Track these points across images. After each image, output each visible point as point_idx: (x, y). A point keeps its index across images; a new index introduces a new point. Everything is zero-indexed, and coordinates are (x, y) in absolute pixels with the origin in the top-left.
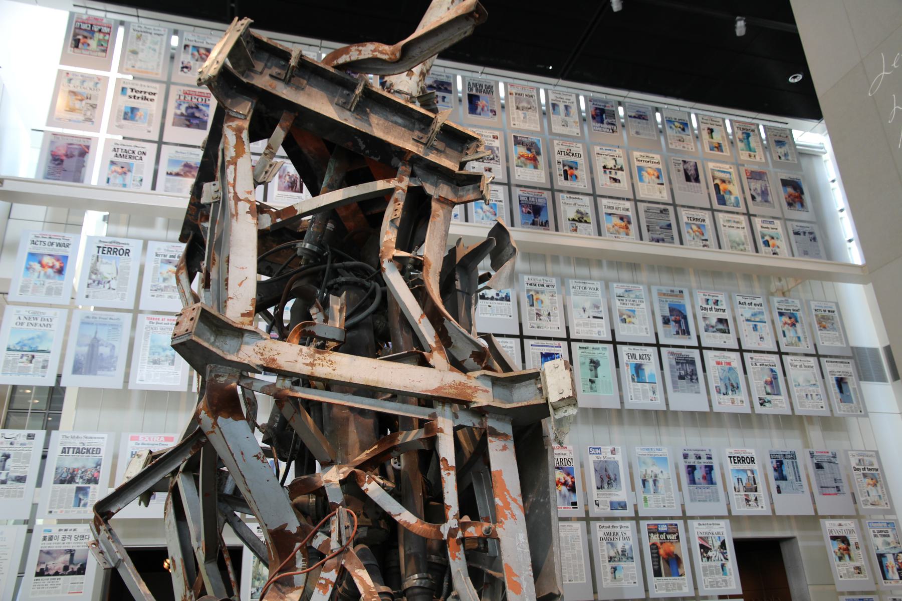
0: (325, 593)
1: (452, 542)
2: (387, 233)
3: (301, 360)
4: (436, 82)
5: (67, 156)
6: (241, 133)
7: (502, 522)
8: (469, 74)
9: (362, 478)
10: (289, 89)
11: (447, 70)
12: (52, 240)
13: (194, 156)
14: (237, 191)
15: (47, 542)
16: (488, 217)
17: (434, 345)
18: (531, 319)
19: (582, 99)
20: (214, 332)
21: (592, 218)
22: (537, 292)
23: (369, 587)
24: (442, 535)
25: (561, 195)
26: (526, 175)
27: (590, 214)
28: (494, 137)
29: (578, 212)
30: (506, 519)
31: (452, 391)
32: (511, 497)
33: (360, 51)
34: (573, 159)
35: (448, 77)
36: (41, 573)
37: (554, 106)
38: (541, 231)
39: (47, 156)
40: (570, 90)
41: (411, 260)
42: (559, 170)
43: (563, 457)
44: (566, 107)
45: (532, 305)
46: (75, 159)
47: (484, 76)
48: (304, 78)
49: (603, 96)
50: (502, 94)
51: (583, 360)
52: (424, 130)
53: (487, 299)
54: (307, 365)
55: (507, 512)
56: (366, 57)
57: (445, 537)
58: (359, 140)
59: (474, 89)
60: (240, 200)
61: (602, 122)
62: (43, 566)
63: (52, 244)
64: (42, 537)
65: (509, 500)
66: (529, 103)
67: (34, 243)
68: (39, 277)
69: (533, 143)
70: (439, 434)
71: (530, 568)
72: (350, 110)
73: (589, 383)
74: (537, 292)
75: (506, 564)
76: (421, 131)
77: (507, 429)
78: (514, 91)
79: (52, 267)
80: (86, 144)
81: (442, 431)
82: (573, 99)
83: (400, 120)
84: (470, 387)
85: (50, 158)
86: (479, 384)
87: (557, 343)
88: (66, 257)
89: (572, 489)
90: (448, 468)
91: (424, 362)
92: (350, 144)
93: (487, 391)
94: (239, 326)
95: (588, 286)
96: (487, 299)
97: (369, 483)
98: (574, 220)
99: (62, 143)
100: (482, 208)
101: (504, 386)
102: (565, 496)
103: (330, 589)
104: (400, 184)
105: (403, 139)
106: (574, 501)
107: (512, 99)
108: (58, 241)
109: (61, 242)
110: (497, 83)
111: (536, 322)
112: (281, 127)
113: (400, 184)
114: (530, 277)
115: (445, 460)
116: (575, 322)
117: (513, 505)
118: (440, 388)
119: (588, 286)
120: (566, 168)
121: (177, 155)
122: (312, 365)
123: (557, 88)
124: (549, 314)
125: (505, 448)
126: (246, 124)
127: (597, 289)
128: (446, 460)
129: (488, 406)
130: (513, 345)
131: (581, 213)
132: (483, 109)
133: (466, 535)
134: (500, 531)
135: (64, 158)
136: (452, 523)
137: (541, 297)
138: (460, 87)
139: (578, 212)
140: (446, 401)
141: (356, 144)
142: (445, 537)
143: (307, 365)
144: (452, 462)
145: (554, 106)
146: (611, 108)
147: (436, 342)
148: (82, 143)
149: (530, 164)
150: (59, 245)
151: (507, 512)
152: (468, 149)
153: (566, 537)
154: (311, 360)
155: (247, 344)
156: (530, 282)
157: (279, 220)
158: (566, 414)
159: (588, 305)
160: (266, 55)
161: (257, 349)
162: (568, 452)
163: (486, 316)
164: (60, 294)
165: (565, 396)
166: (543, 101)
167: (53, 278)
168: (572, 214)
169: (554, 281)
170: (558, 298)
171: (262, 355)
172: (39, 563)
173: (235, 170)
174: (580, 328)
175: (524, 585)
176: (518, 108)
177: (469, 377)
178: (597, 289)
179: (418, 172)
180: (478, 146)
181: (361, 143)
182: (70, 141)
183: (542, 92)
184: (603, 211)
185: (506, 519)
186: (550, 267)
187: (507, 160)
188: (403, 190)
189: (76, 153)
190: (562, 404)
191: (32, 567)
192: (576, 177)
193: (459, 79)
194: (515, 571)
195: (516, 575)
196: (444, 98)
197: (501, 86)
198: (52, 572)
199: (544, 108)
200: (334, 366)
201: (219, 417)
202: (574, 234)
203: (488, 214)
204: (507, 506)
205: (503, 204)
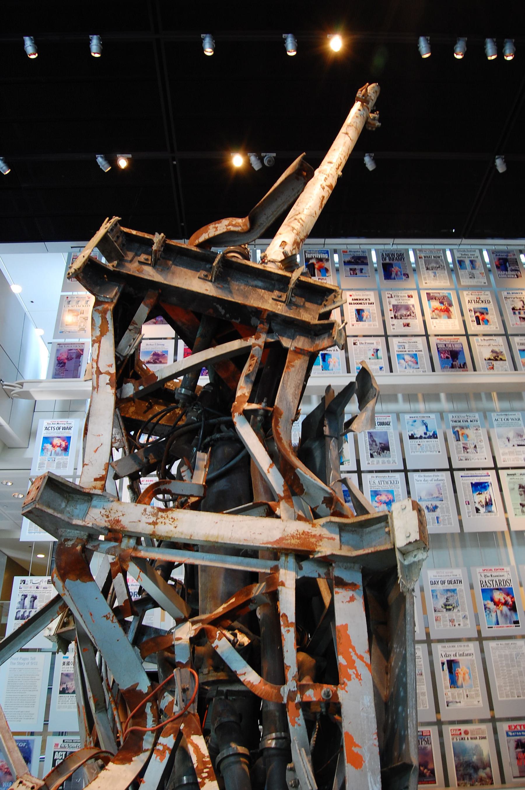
0: (162, 760)
1: (291, 707)
2: (241, 387)
3: (144, 519)
4: (353, 257)
5: (67, 359)
6: (106, 314)
7: (344, 683)
8: (382, 247)
9: (213, 634)
10: (154, 271)
11: (362, 247)
12: (59, 426)
13: (160, 346)
14: (99, 366)
15: (66, 666)
16: (410, 366)
17: (282, 494)
18: (458, 453)
19: (485, 253)
20: (66, 498)
21: (506, 355)
22: (462, 428)
23: (204, 756)
24: (282, 698)
25: (475, 338)
26: (441, 325)
27: (504, 352)
28: (409, 297)
29: (493, 351)
30: (349, 679)
31: (293, 541)
32: (356, 654)
33: (216, 228)
34: (483, 305)
35: (363, 252)
36: (63, 692)
37: (461, 262)
38: (461, 373)
39: (54, 361)
40: (473, 247)
41: (261, 412)
42: (470, 318)
43: (501, 578)
44: (472, 262)
45: (458, 440)
46: (74, 360)
47: (395, 247)
48: (170, 260)
49: (505, 248)
50: (412, 259)
51: (512, 486)
52: (284, 289)
53: (417, 438)
54: (150, 524)
55: (350, 671)
56: (221, 232)
57: (285, 701)
58: (218, 306)
59: (387, 258)
60: (101, 373)
61: (506, 270)
62: (64, 686)
63: (59, 428)
64: (62, 663)
65: (354, 657)
66: (437, 263)
67: (47, 429)
68: (51, 455)
69: (444, 297)
70: (280, 588)
71: (375, 736)
72: (211, 281)
73: (520, 507)
74: (462, 428)
75: (347, 733)
76: (280, 290)
77: (357, 578)
78: (422, 255)
79: (60, 446)
80: (81, 348)
81: (283, 584)
82: (477, 253)
83: (260, 284)
84: (314, 536)
85: (57, 362)
86: (325, 532)
87: (485, 472)
88: (69, 438)
89: (513, 608)
90: (288, 625)
91: (271, 513)
92: (211, 311)
93: (333, 539)
94: (87, 491)
95: (509, 417)
96: (417, 438)
97: (220, 639)
98: (489, 359)
99: (64, 349)
100: (404, 359)
101: (353, 532)
102: (506, 616)
103: (168, 755)
104: (256, 342)
105: (268, 302)
106: (515, 620)
107: (422, 262)
108: (63, 426)
109: (66, 426)
110: (407, 251)
111: (463, 455)
112: (145, 304)
113: (256, 342)
114: (454, 415)
115: (285, 615)
116: (501, 451)
117: (358, 663)
118: (282, 539)
119: (509, 417)
120: (478, 314)
121: (147, 347)
122: (155, 523)
123: (461, 247)
124: (475, 447)
125: (352, 599)
126: (111, 307)
127: (519, 419)
128: (286, 616)
129: (332, 555)
130: (444, 478)
131: (496, 352)
132: (396, 274)
133: (305, 699)
134: (342, 695)
135: (66, 361)
136: (291, 685)
137: (466, 431)
138: (374, 259)
139: (493, 351)
140: (287, 552)
141: (216, 310)
142: (285, 701)
143: (150, 524)
144: (292, 618)
145: (461, 262)
146: (513, 257)
147: (284, 491)
148: (78, 348)
149: (444, 315)
150: (64, 428)
151: (350, 671)
152: (327, 300)
153: (511, 655)
154: (154, 519)
155: (95, 507)
156: (454, 419)
157: (141, 388)
158: (416, 559)
159: (511, 435)
160: (137, 245)
161: (103, 512)
162: (505, 574)
163: (416, 453)
164: (66, 467)
165: (412, 539)
166: (450, 260)
167: (61, 455)
168: (488, 355)
169: (477, 416)
170: (483, 432)
171: (108, 517)
172: (62, 683)
173: (99, 347)
174: (507, 457)
175: (367, 758)
176: (427, 269)
177: (314, 525)
178: (519, 419)
179: (275, 327)
180: (335, 297)
181: (220, 309)
182: (70, 348)
183: (448, 253)
184: (516, 348)
185: (349, 679)
186: (473, 404)
187: (423, 315)
188: (260, 346)
189: (74, 356)
190: (410, 548)
191: (56, 687)
192: (488, 321)
193: (373, 253)
194: (356, 740)
195: (356, 745)
196: (361, 270)
197: (411, 253)
198: (71, 691)
199: (451, 266)
200: (176, 523)
201: (67, 580)
202: (491, 372)
203: (410, 363)
204: (351, 664)
205: (423, 353)
